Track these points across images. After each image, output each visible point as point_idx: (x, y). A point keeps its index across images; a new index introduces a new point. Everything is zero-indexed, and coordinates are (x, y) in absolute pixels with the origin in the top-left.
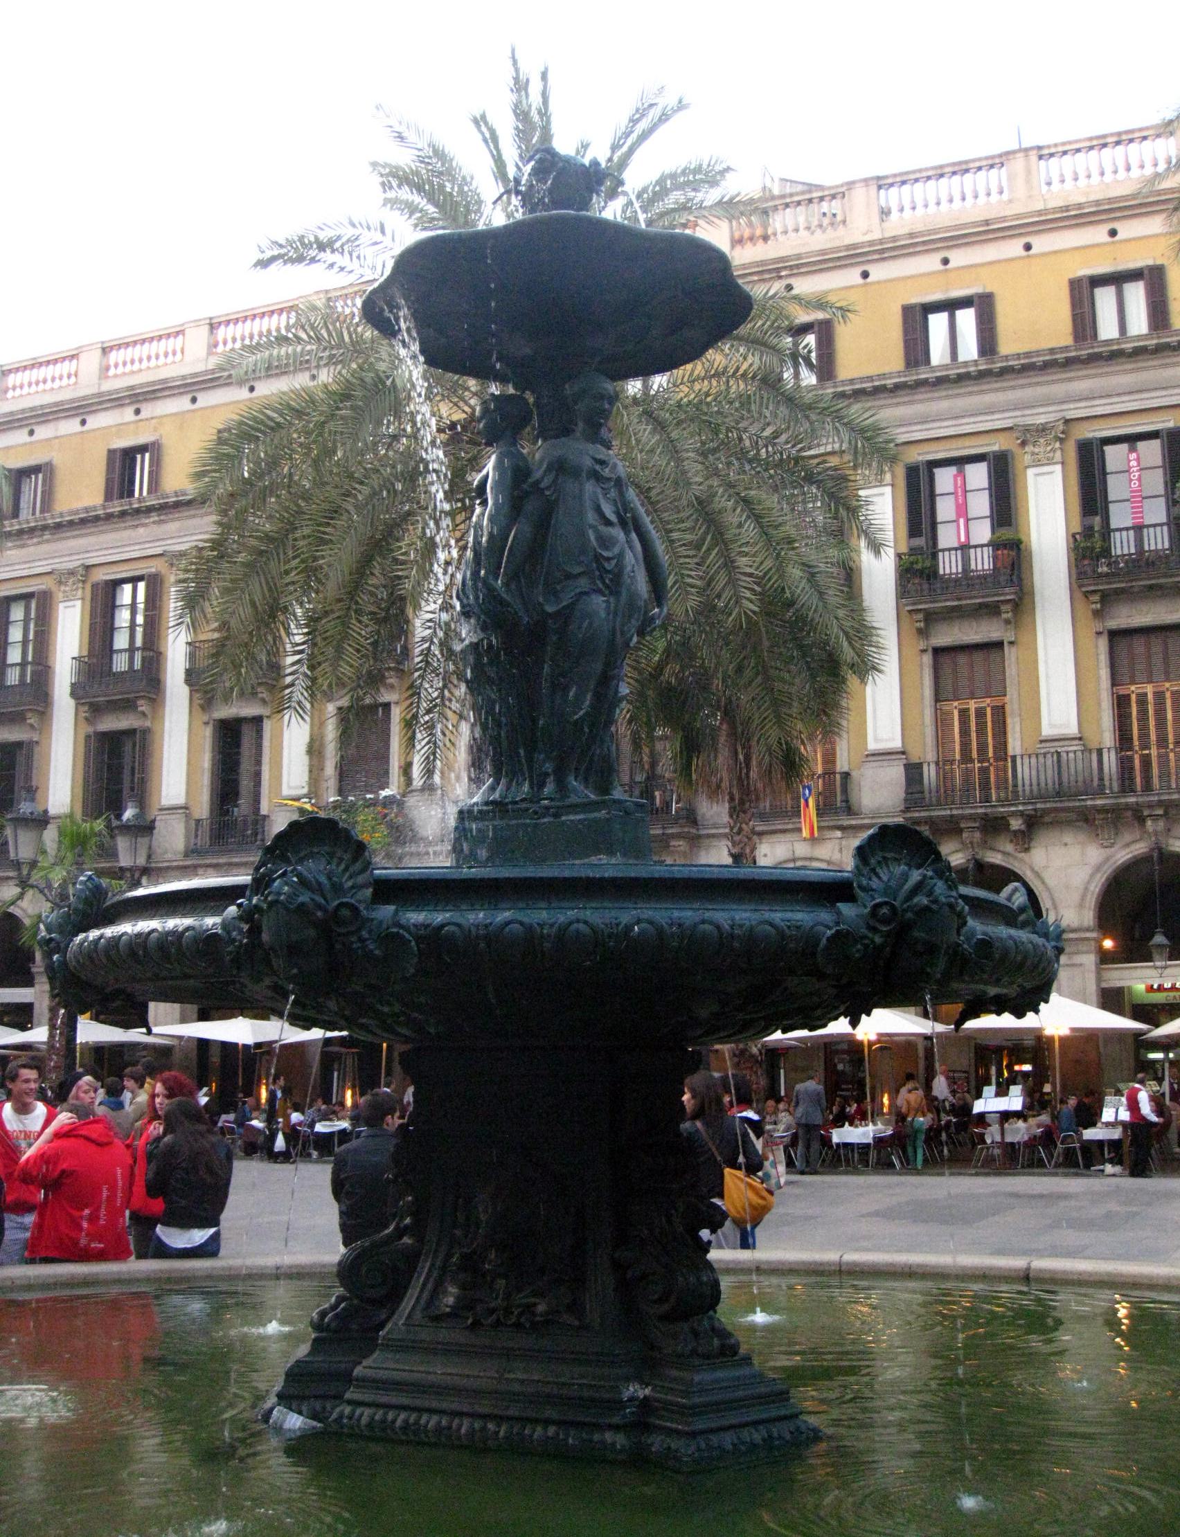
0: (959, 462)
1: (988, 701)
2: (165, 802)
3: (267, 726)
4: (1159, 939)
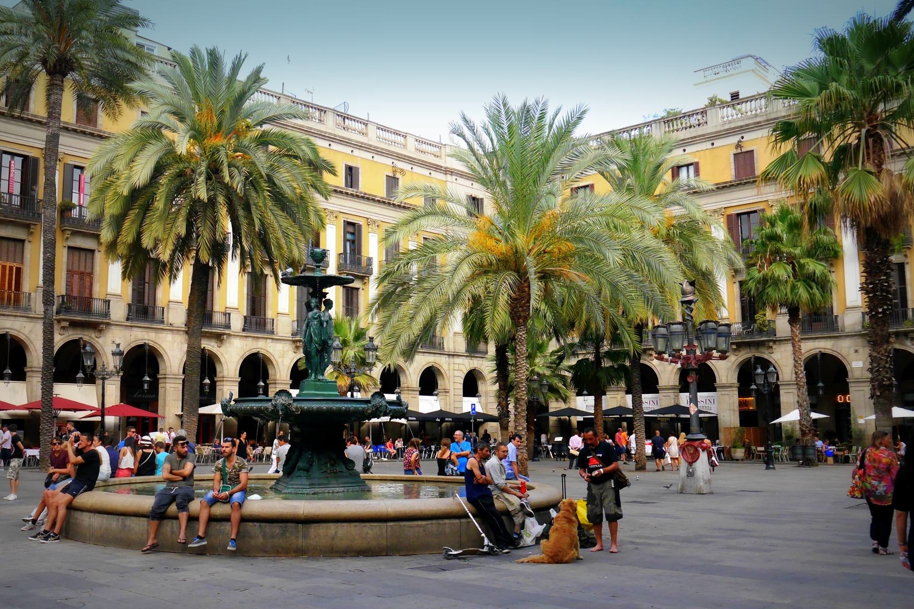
0: (13, 155)
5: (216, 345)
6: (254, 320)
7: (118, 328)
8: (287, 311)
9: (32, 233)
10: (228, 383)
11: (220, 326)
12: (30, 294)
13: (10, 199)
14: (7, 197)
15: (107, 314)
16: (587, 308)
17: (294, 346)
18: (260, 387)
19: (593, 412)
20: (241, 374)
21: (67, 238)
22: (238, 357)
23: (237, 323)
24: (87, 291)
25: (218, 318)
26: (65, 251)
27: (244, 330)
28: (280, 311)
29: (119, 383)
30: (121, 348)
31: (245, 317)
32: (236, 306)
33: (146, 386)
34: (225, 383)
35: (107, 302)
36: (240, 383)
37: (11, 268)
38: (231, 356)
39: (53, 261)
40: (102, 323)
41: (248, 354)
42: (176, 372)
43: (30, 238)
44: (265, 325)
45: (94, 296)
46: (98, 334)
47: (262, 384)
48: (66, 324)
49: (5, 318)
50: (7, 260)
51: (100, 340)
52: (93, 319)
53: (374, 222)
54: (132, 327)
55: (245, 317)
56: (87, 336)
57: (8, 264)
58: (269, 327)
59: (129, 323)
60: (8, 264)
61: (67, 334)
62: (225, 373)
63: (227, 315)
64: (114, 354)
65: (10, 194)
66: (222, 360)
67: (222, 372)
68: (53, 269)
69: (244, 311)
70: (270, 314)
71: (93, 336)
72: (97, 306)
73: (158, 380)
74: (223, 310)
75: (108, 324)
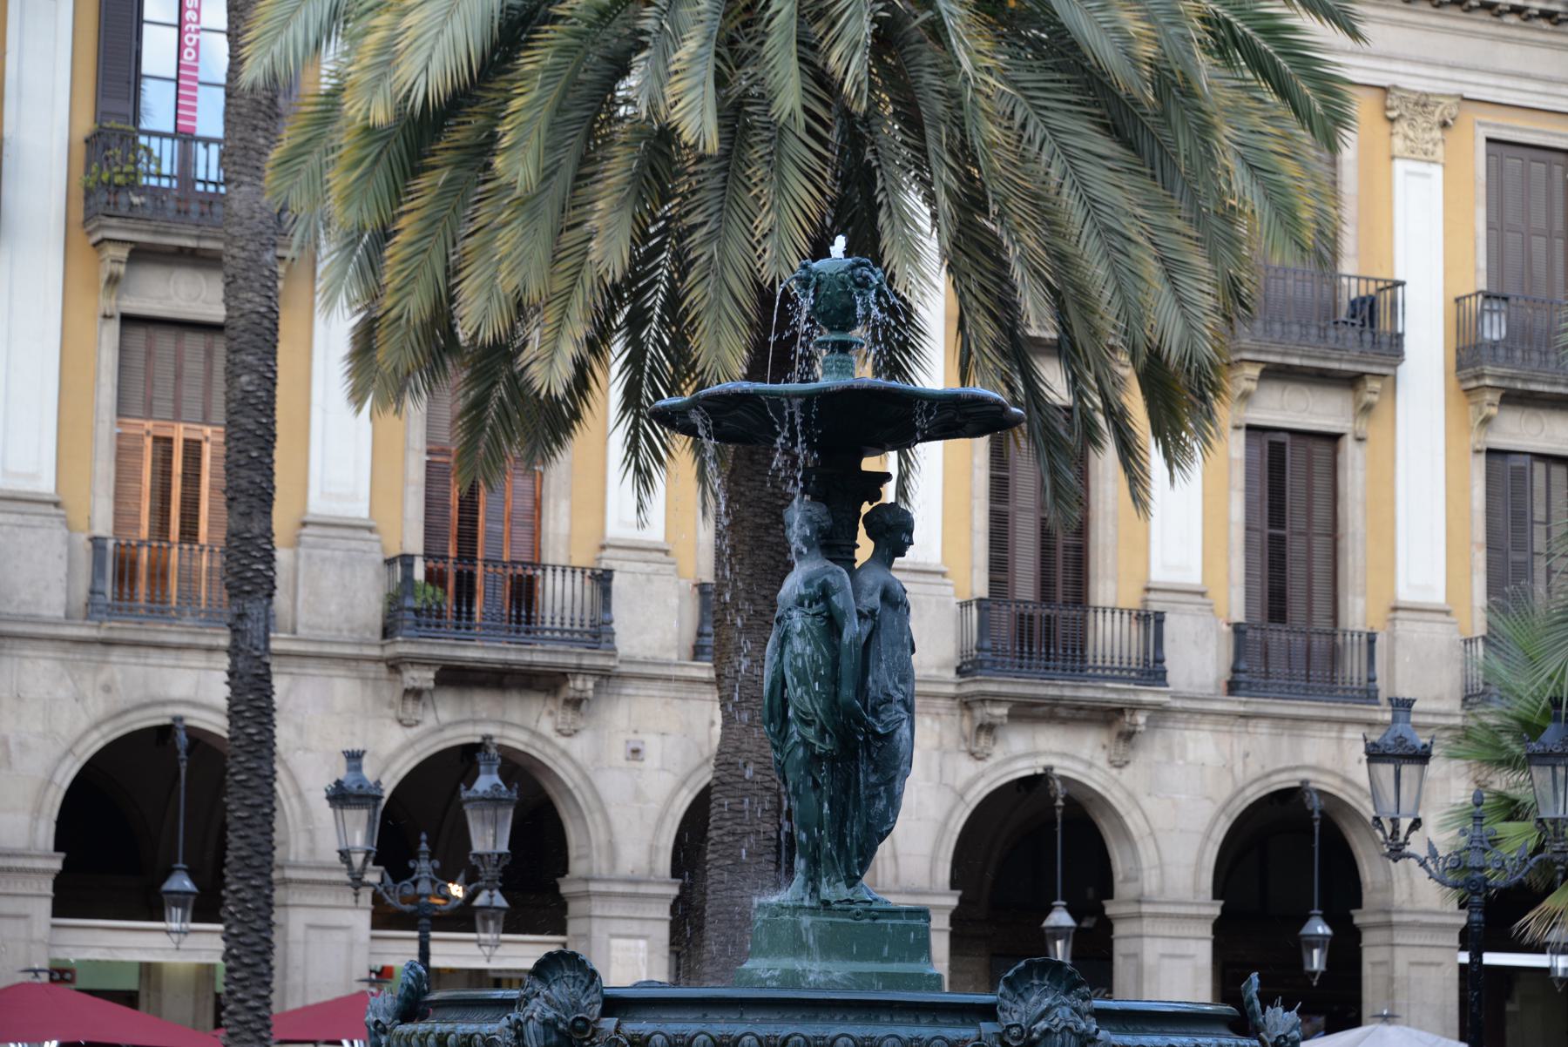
1: (149, 425)
2: (318, 505)
3: (1353, 458)
4: (181, 882)
5: (1101, 759)
6: (1278, 637)
7: (654, 689)
8: (1438, 598)
9: (1368, 409)
10: (1163, 928)
11: (568, 637)
12: (1371, 639)
13: (186, 162)
14: (166, 152)
15: (599, 633)
16: (1525, 381)
17: (391, 692)
18: (1315, 942)
19: (615, 942)
20: (1221, 888)
21: (1487, 421)
22: (1207, 811)
23: (1198, 656)
24: (522, 535)
25: (1110, 635)
26: (1241, 436)
27: (1233, 688)
28: (1405, 595)
29: (662, 932)
30: (369, 772)
31: (1238, 629)
32: (1194, 578)
33: (1060, 951)
34: (1147, 926)
35: (603, 580)
36: (1221, 928)
37: (164, 444)
38: (1172, 806)
39: (269, 406)
40: (580, 670)
41: (1253, 794)
42: (922, 882)
43: (1363, 426)
44: (1334, 656)
45: (549, 557)
46: (567, 717)
47: (1322, 929)
48: (423, 677)
49: (168, 658)
50: (177, 417)
51: (579, 747)
52: (537, 656)
53: (1423, 102)
54: (108, 643)
55: (1238, 629)
56: (522, 725)
57: (179, 433)
58: (1353, 666)
59: (1235, 705)
60: (179, 433)
61: (429, 721)
62: (1150, 883)
63: (1151, 622)
64: (340, 796)
65: (185, 137)
66: (1133, 821)
67: (1132, 879)
68: (268, 440)
69: (1234, 603)
70: (1357, 612)
71: (546, 726)
72: (560, 595)
73: (1106, 925)
74: (1132, 600)
75: (605, 677)
